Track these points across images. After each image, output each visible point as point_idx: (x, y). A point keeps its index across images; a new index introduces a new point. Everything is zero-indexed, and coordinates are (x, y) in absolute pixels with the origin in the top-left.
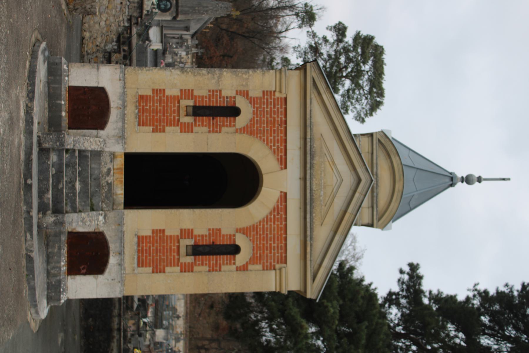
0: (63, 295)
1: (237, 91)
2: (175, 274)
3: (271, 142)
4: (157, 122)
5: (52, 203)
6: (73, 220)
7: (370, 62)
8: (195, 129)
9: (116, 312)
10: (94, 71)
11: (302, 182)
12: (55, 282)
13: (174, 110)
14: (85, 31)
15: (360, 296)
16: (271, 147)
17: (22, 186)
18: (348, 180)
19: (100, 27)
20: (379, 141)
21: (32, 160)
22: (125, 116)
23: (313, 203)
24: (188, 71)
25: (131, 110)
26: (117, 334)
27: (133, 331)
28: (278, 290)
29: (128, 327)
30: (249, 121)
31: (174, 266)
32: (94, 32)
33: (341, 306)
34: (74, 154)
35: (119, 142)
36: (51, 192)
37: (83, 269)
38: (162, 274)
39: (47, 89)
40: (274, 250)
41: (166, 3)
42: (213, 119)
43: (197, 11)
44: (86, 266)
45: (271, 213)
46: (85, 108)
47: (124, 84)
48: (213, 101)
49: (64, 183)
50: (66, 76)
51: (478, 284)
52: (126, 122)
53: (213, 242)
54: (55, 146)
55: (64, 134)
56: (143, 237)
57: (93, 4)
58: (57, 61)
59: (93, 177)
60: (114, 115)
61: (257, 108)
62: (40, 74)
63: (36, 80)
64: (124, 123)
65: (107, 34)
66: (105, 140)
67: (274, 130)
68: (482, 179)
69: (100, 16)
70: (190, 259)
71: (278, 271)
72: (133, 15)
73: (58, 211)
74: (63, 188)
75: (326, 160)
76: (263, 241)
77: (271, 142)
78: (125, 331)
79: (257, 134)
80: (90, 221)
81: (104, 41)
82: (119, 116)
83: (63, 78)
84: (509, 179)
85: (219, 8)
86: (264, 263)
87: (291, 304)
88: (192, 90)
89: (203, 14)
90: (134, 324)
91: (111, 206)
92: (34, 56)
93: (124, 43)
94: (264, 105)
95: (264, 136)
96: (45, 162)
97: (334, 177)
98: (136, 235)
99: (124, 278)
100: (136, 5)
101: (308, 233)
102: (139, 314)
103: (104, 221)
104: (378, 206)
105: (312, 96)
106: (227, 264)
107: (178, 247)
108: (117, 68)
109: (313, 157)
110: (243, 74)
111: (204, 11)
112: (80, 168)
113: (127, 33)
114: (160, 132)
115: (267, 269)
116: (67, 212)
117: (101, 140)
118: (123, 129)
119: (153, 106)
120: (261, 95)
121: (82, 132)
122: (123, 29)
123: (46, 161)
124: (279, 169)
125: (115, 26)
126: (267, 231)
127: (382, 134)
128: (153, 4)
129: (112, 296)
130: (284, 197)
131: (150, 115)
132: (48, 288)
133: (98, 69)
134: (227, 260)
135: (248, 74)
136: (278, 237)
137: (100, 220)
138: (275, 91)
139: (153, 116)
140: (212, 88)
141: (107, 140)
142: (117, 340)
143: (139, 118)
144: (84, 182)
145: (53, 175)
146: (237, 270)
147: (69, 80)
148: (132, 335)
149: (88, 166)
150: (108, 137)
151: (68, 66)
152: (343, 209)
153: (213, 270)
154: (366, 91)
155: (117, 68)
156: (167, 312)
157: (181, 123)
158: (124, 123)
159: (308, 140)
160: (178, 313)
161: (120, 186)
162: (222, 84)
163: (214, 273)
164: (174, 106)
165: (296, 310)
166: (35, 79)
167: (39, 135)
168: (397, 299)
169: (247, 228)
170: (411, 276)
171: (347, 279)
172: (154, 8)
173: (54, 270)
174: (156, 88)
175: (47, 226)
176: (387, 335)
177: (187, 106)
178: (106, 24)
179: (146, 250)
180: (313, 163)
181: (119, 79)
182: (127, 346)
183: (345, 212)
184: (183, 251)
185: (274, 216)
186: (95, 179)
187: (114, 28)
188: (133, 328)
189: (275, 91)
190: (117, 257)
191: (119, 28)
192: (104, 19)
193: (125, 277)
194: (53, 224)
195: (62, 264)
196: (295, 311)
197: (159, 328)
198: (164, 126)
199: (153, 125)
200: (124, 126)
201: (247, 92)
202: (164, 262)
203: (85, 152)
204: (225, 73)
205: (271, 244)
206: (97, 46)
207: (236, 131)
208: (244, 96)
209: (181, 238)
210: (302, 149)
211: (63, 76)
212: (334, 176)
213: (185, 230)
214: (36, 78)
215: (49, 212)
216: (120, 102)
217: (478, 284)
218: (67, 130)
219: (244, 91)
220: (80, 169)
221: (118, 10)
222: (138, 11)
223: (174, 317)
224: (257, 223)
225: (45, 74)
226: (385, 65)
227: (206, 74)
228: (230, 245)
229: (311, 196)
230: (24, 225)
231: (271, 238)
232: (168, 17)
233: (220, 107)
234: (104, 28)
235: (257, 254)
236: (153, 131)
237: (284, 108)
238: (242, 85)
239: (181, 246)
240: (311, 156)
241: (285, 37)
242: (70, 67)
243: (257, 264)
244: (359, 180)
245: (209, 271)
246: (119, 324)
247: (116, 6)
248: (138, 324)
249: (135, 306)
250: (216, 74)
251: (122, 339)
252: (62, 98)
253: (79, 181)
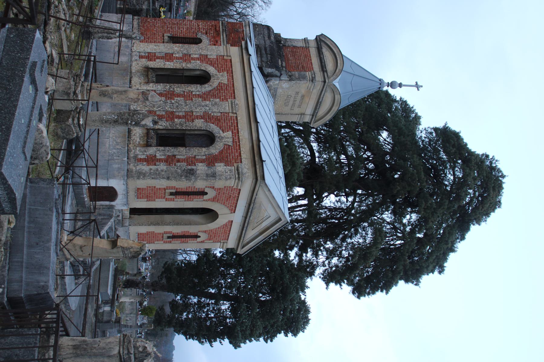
11: (244, 218)
71: (222, 244)
133: (108, 180)
153: (183, 242)
216: (125, 200)
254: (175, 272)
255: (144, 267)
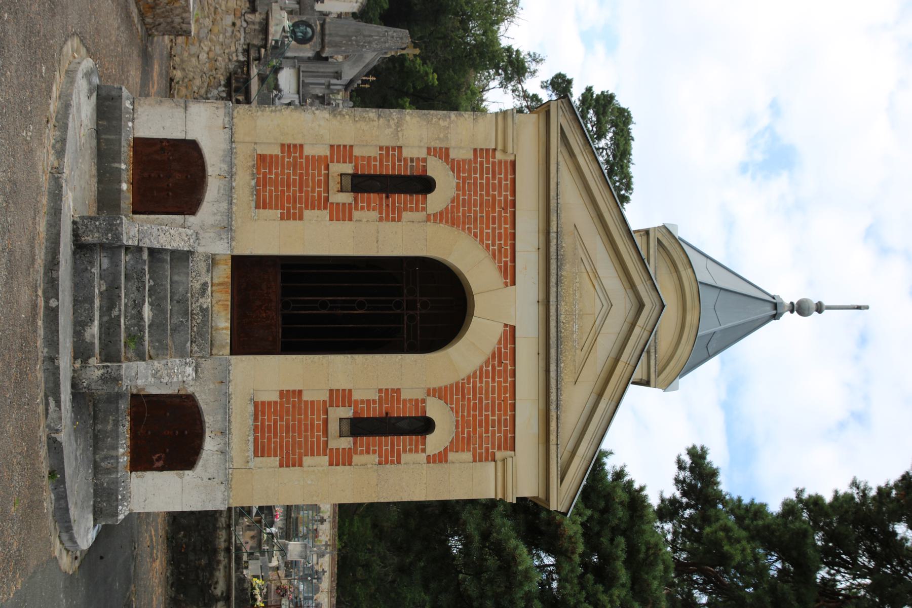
0: (123, 506)
1: (429, 149)
3: (488, 239)
4: (289, 202)
5: (100, 343)
6: (137, 374)
8: (356, 214)
11: (542, 308)
12: (108, 483)
13: (320, 181)
14: (174, 68)
16: (488, 246)
17: (41, 312)
18: (622, 305)
19: (199, 61)
20: (659, 241)
21: (59, 262)
22: (233, 190)
23: (561, 345)
24: (344, 113)
25: (244, 181)
28: (499, 496)
31: (319, 454)
32: (189, 70)
34: (141, 256)
35: (222, 237)
36: (96, 323)
37: (157, 460)
39: (94, 142)
42: (387, 197)
43: (354, 43)
45: (487, 363)
48: (387, 166)
49: (123, 308)
50: (129, 121)
52: (234, 201)
53: (387, 414)
54: (105, 240)
55: (121, 219)
56: (263, 403)
57: (184, 15)
59: (176, 298)
61: (464, 178)
64: (231, 203)
65: (210, 73)
66: (197, 233)
67: (494, 217)
69: (200, 45)
70: (346, 443)
71: (500, 464)
72: (252, 43)
74: (119, 317)
75: (584, 270)
76: (475, 410)
77: (488, 239)
78: (238, 549)
79: (464, 223)
80: (169, 375)
81: (206, 85)
82: (222, 191)
83: (123, 123)
84: (867, 308)
86: (474, 449)
88: (351, 147)
93: (237, 90)
94: (475, 173)
95: (475, 228)
96: (87, 269)
97: (598, 300)
98: (251, 400)
100: (257, 27)
101: (553, 397)
104: (658, 351)
105: (559, 159)
106: (411, 451)
107: (326, 421)
108: (220, 106)
109: (562, 264)
110: (439, 119)
112: (151, 281)
114: (294, 219)
115: (481, 461)
118: (229, 214)
119: (283, 174)
120: (471, 156)
121: (158, 218)
123: (89, 268)
124: (503, 285)
125: (224, 60)
126: (481, 393)
127: (664, 231)
128: (284, 30)
130: (511, 333)
131: (276, 191)
133: (186, 108)
134: (411, 444)
135: (448, 120)
136: (500, 404)
138: (495, 150)
139: (283, 191)
140: (385, 143)
141: (201, 232)
142: (225, 567)
143: (258, 195)
144: (157, 306)
145: (101, 293)
146: (428, 462)
147: (135, 127)
151: (133, 104)
155: (220, 106)
157: (332, 204)
158: (231, 203)
161: (223, 313)
162: (403, 136)
163: (388, 466)
167: (75, 219)
169: (446, 387)
172: (287, 37)
173: (106, 463)
174: (287, 142)
177: (341, 175)
178: (208, 58)
179: (269, 426)
180: (562, 275)
182: (242, 573)
183: (617, 360)
184: (334, 427)
185: (493, 366)
187: (221, 63)
188: (251, 543)
189: (495, 150)
190: (219, 440)
191: (229, 63)
192: (206, 49)
193: (232, 474)
194: (100, 382)
195: (121, 451)
198: (301, 209)
199: (282, 208)
200: (232, 208)
201: (447, 149)
202: (300, 448)
203: (161, 253)
204: (408, 118)
205: (487, 416)
208: (440, 158)
209: (331, 406)
210: (542, 251)
211: (123, 119)
213: (338, 390)
216: (225, 167)
218: (131, 215)
219: (441, 149)
220: (152, 283)
221: (228, 34)
222: (261, 36)
223: (316, 521)
224: (463, 380)
225: (92, 115)
227: (376, 119)
228: (416, 418)
230: (43, 385)
232: (307, 51)
233: (400, 177)
235: (463, 433)
236: (282, 219)
238: (438, 139)
239: (329, 420)
240: (557, 262)
242: (136, 105)
243: (463, 450)
245: (380, 463)
247: (225, 29)
250: (393, 120)
252: (122, 158)
254: (95, 270)
255: (132, 262)
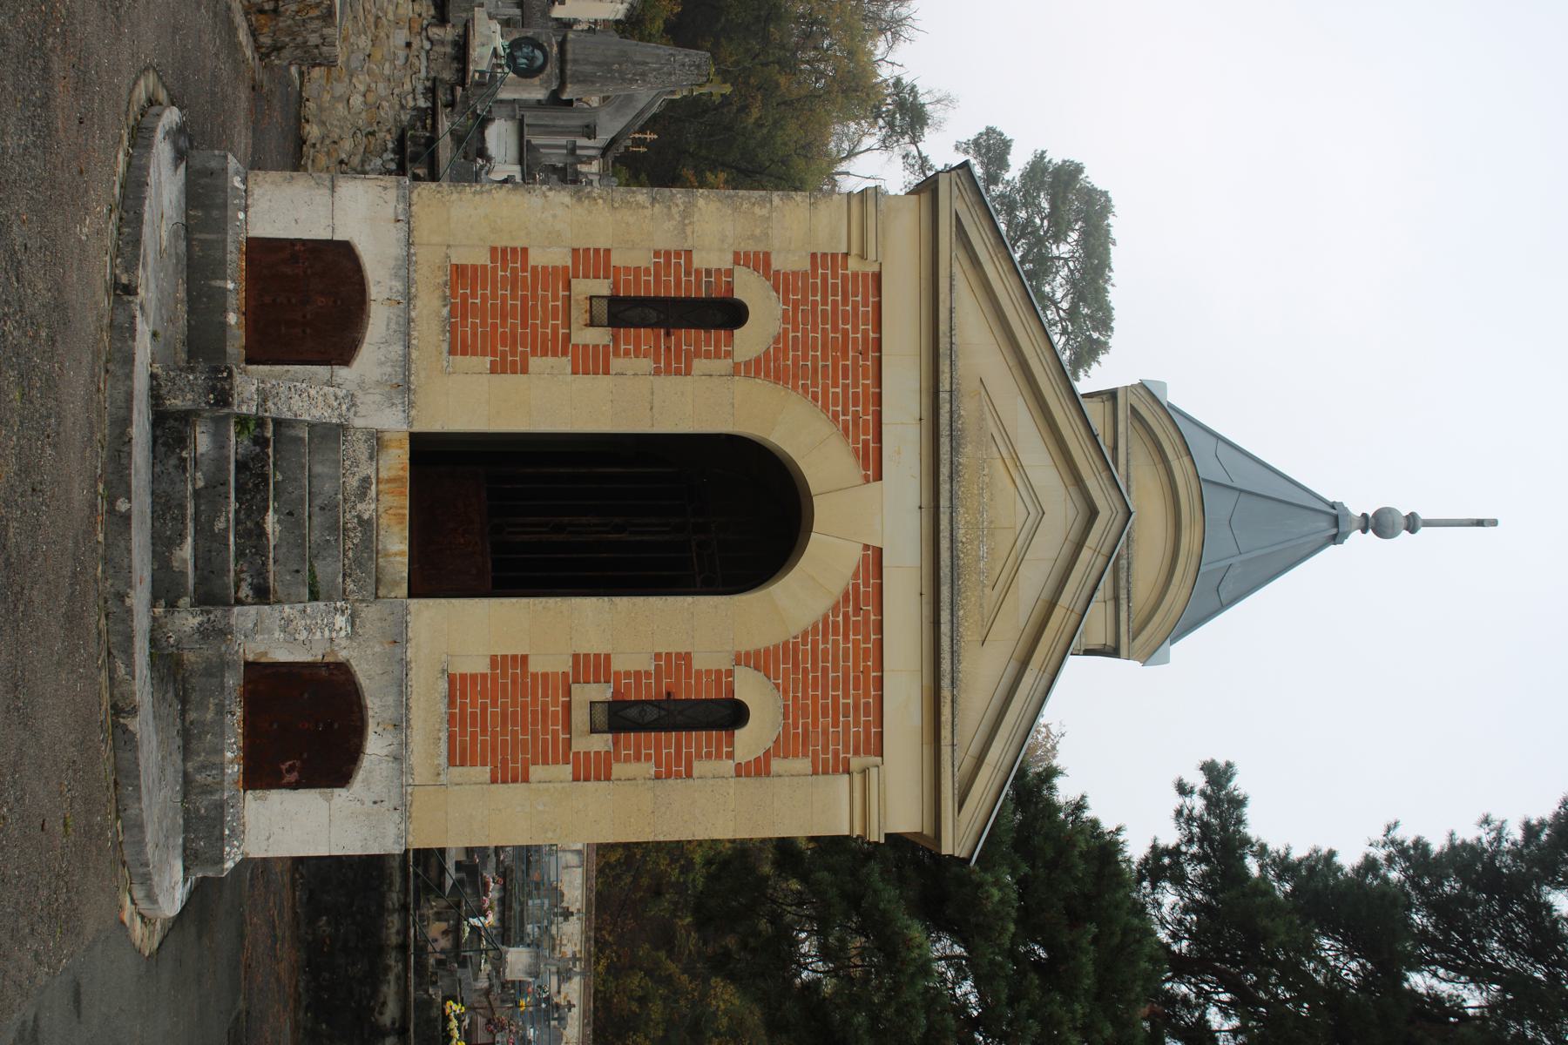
1: (736, 254)
2: (559, 786)
3: (836, 404)
4: (504, 344)
7: (1074, 236)
8: (616, 364)
9: (394, 898)
10: (322, 195)
13: (555, 308)
14: (308, 121)
15: (1076, 853)
16: (835, 415)
19: (349, 109)
25: (430, 308)
26: (396, 961)
27: (442, 951)
28: (857, 832)
29: (427, 941)
30: (771, 341)
31: (556, 762)
32: (332, 125)
33: (1022, 882)
36: (189, 540)
37: (290, 770)
38: (520, 786)
39: (182, 245)
40: (846, 715)
41: (533, 51)
42: (668, 335)
44: (298, 764)
45: (835, 609)
46: (294, 301)
47: (410, 231)
49: (232, 516)
51: (1396, 824)
52: (413, 342)
53: (669, 694)
56: (463, 677)
58: (213, 164)
59: (318, 502)
60: (379, 321)
61: (796, 303)
62: (159, 195)
63: (147, 208)
64: (408, 346)
65: (369, 129)
67: (845, 368)
68: (1420, 523)
69: (350, 81)
70: (601, 743)
71: (857, 778)
73: (210, 597)
74: (227, 530)
77: (836, 404)
78: (421, 951)
79: (795, 377)
80: (309, 630)
82: (393, 326)
83: (230, 213)
84: (1494, 523)
85: (677, 66)
86: (815, 753)
87: (876, 876)
88: (608, 251)
89: (634, 81)
90: (445, 933)
91: (371, 588)
92: (140, 136)
93: (415, 158)
94: (815, 295)
95: (815, 385)
98: (443, 671)
99: (409, 798)
101: (946, 665)
102: (458, 906)
103: (349, 629)
106: (709, 755)
107: (568, 707)
109: (959, 445)
111: (634, 74)
112: (278, 473)
113: (424, 127)
115: (825, 772)
116: (239, 602)
117: (341, 393)
119: (494, 295)
120: (807, 266)
122: (412, 116)
124: (861, 481)
125: (391, 107)
128: (495, 53)
129: (375, 850)
130: (875, 559)
131: (484, 323)
132: (187, 828)
133: (333, 189)
134: (709, 745)
136: (856, 679)
137: (337, 627)
138: (846, 255)
139: (494, 326)
140: (662, 246)
141: (359, 394)
142: (398, 978)
143: (453, 332)
146: (738, 775)
148: (440, 963)
149: (303, 467)
150: (360, 386)
151: (245, 181)
152: (1046, 595)
153: (669, 776)
154: (1064, 311)
155: (388, 185)
156: (538, 901)
157: (576, 346)
158: (408, 346)
159: (944, 396)
160: (565, 904)
161: (396, 529)
162: (693, 233)
163: (671, 781)
164: (555, 298)
165: (891, 892)
166: (142, 205)
167: (155, 371)
168: (1176, 864)
169: (767, 650)
170: (1212, 802)
171: (1037, 804)
172: (500, 66)
174: (500, 244)
175: (179, 641)
176: (1152, 959)
177: (591, 298)
179: (473, 714)
180: (960, 464)
181: (392, 217)
183: (1052, 605)
184: (580, 717)
185: (846, 616)
186: (322, 509)
187: (387, 112)
189: (846, 255)
190: (389, 737)
191: (402, 112)
192: (362, 88)
193: (411, 794)
195: (229, 755)
196: (889, 897)
197: (516, 945)
199: (494, 354)
200: (409, 354)
201: (767, 255)
202: (525, 752)
204: (701, 202)
206: (341, 162)
207: (736, 370)
209: (576, 681)
212: (1018, 498)
213: (587, 656)
214: (147, 202)
215: (185, 601)
216: (398, 285)
217: (1396, 824)
218: (242, 365)
219: (756, 254)
220: (279, 477)
223: (556, 915)
224: (795, 637)
226: (1114, 244)
227: (648, 205)
229: (953, 557)
231: (836, 679)
232: (536, 92)
234: (360, 113)
236: (493, 371)
237: (873, 302)
238: (753, 236)
241: (848, 173)
242: (251, 183)
243: (796, 755)
244: (1093, 513)
245: (658, 777)
246: (404, 931)
248: (456, 931)
249: (449, 883)
251: (411, 975)
253: (275, 511)
